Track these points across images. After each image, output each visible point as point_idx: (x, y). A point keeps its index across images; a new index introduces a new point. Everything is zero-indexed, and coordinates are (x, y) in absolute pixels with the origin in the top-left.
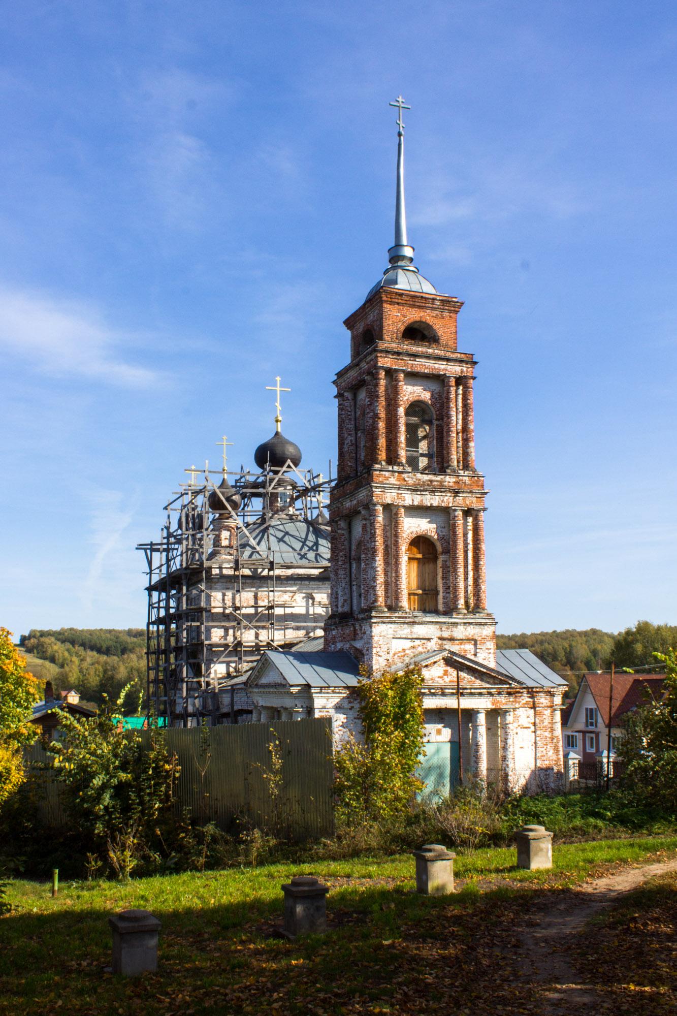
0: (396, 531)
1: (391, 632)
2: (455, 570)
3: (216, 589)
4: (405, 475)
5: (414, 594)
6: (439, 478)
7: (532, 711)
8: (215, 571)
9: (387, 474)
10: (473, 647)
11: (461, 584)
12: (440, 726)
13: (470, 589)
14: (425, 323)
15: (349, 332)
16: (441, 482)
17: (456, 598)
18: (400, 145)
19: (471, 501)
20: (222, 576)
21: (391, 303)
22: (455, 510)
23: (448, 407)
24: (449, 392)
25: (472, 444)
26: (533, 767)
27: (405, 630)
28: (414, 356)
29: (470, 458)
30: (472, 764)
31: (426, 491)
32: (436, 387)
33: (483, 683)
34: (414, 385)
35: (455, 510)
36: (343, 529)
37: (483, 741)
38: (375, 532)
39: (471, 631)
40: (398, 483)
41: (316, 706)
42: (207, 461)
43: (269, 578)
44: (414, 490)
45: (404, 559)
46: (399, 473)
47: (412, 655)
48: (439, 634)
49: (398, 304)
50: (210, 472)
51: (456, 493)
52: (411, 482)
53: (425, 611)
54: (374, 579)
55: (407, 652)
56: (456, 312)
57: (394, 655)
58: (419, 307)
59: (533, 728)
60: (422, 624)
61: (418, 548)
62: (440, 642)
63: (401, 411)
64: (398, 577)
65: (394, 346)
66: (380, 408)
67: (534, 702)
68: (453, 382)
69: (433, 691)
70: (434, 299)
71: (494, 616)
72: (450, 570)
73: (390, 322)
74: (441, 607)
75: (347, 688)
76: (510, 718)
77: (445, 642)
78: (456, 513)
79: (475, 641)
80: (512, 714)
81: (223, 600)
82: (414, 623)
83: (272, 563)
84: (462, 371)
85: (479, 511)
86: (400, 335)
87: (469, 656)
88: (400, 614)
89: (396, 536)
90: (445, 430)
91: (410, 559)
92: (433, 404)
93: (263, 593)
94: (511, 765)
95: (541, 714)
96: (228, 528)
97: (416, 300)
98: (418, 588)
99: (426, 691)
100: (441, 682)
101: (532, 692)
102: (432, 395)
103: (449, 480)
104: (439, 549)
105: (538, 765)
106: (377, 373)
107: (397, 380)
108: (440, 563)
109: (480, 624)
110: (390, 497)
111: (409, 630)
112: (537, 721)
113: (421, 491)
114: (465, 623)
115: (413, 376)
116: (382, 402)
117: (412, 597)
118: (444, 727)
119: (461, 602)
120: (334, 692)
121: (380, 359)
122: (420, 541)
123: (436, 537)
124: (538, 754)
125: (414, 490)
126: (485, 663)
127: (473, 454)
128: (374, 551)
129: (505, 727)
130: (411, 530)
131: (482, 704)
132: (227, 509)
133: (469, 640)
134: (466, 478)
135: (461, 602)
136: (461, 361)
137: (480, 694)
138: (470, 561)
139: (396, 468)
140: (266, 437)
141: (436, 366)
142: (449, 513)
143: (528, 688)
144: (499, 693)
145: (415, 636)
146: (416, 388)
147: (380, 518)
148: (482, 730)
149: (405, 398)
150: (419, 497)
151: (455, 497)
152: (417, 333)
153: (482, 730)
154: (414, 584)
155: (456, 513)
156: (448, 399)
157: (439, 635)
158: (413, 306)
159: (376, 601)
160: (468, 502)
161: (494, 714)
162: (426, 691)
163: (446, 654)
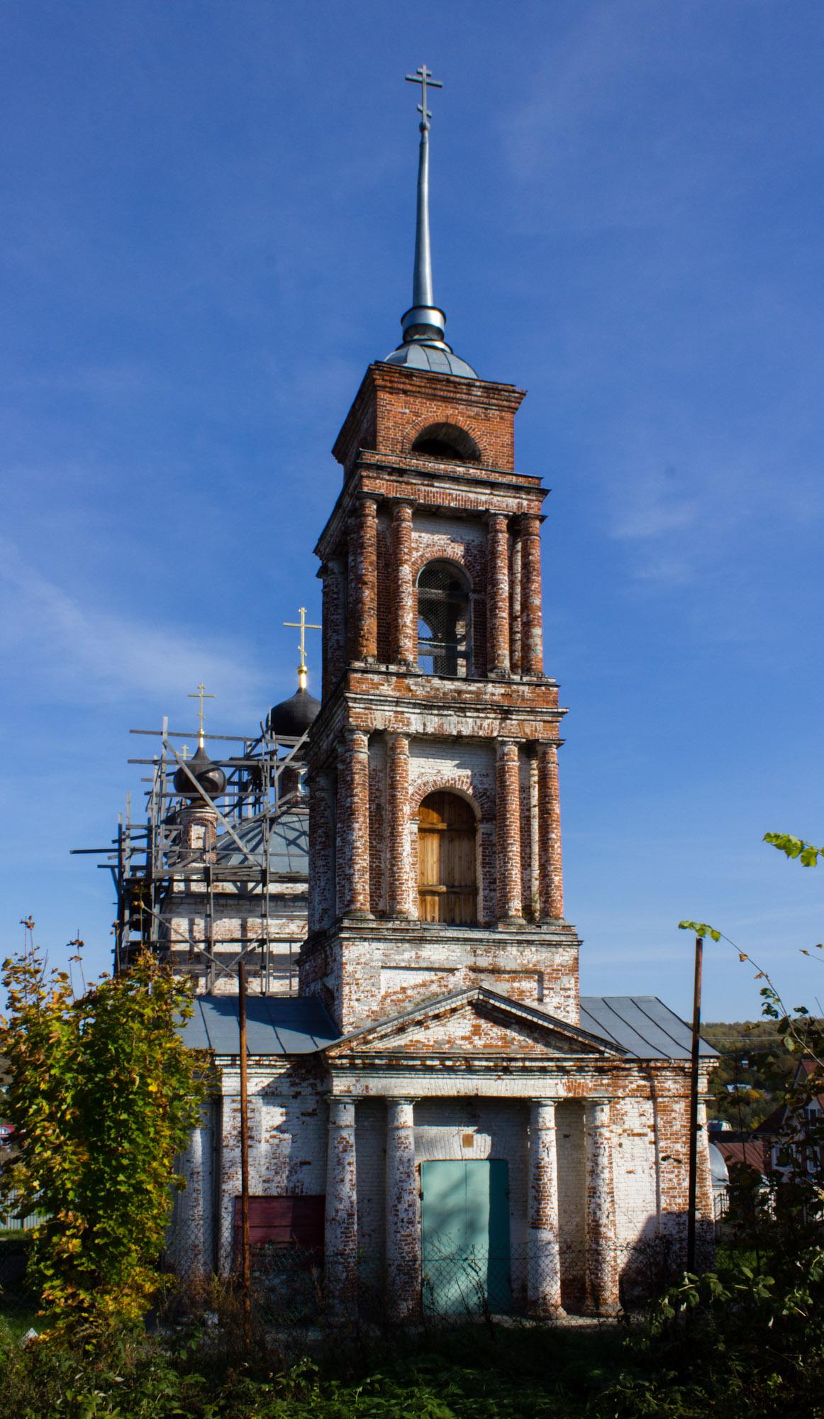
0: (393, 778)
1: (378, 955)
2: (504, 849)
3: (180, 915)
4: (410, 681)
5: (433, 893)
6: (473, 687)
7: (648, 1106)
8: (179, 887)
9: (376, 678)
10: (535, 985)
11: (516, 873)
12: (470, 1130)
13: (536, 885)
14: (455, 428)
15: (341, 467)
16: (478, 693)
17: (505, 899)
18: (422, 145)
19: (536, 729)
20: (189, 894)
21: (392, 391)
22: (504, 743)
23: (494, 568)
24: (495, 542)
25: (537, 631)
26: (652, 1210)
27: (407, 954)
28: (432, 477)
29: (533, 655)
30: (531, 1202)
31: (449, 708)
32: (473, 536)
33: (550, 1050)
34: (433, 533)
35: (504, 743)
36: (322, 789)
37: (550, 1158)
38: (353, 780)
39: (532, 956)
40: (398, 694)
41: (225, 1091)
42: (166, 719)
43: (261, 897)
44: (427, 706)
45: (408, 830)
46: (398, 675)
47: (419, 998)
48: (470, 961)
49: (405, 392)
50: (170, 734)
51: (505, 713)
52: (420, 692)
53: (451, 922)
54: (351, 862)
55: (409, 992)
56: (513, 410)
57: (384, 998)
58: (445, 400)
59: (651, 1136)
60: (437, 942)
61: (441, 813)
62: (472, 975)
63: (406, 572)
64: (395, 858)
65: (393, 460)
66: (365, 565)
67: (652, 1088)
68: (503, 524)
69: (449, 1063)
70: (469, 385)
71: (575, 930)
72: (496, 849)
73: (391, 425)
74: (481, 916)
75: (285, 1057)
76: (603, 1116)
77: (482, 976)
78: (506, 749)
79: (541, 976)
80: (606, 1108)
81: (191, 931)
82: (422, 940)
83: (264, 872)
84: (520, 506)
85: (548, 745)
86: (408, 446)
87: (528, 1002)
88: (397, 924)
89: (393, 786)
90: (488, 606)
91: (421, 830)
92: (469, 565)
93: (254, 922)
94: (606, 1206)
95: (666, 1110)
96: (202, 822)
97: (439, 386)
98: (440, 882)
99: (436, 1063)
100: (467, 1046)
101: (648, 1069)
102: (467, 550)
103: (494, 691)
104: (478, 813)
105: (663, 1205)
106: (363, 507)
107: (400, 519)
108: (479, 838)
109: (549, 944)
110: (381, 718)
111: (413, 954)
112: (660, 1123)
113: (439, 708)
114: (520, 942)
115: (430, 515)
116: (371, 555)
117: (429, 898)
118: (478, 1131)
119: (516, 905)
120: (259, 1065)
121: (366, 482)
122: (439, 800)
123: (470, 791)
124: (662, 1185)
125: (426, 707)
126: (560, 1015)
127: (539, 648)
128: (350, 814)
129: (594, 1132)
130: (425, 779)
131: (549, 1088)
132: (197, 791)
133: (528, 973)
134: (526, 688)
135: (516, 905)
136: (517, 488)
137: (543, 1070)
138: (536, 836)
139: (393, 668)
140: (285, 696)
141: (472, 496)
142: (494, 750)
143: (638, 1061)
144: (581, 1070)
145: (424, 965)
146: (436, 537)
147: (363, 755)
148: (550, 1137)
149: (415, 555)
150: (436, 719)
151: (503, 720)
152: (443, 443)
153: (550, 1137)
154: (433, 876)
155: (506, 749)
156: (494, 555)
157: (470, 963)
158: (433, 397)
159: (352, 901)
160: (528, 730)
161: (574, 1111)
162: (436, 1063)
163: (475, 994)
